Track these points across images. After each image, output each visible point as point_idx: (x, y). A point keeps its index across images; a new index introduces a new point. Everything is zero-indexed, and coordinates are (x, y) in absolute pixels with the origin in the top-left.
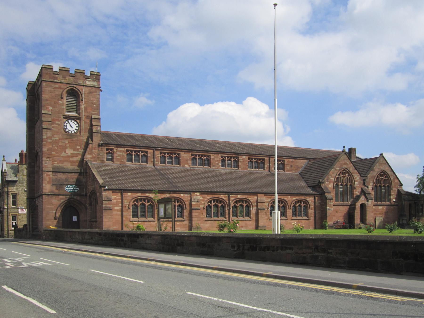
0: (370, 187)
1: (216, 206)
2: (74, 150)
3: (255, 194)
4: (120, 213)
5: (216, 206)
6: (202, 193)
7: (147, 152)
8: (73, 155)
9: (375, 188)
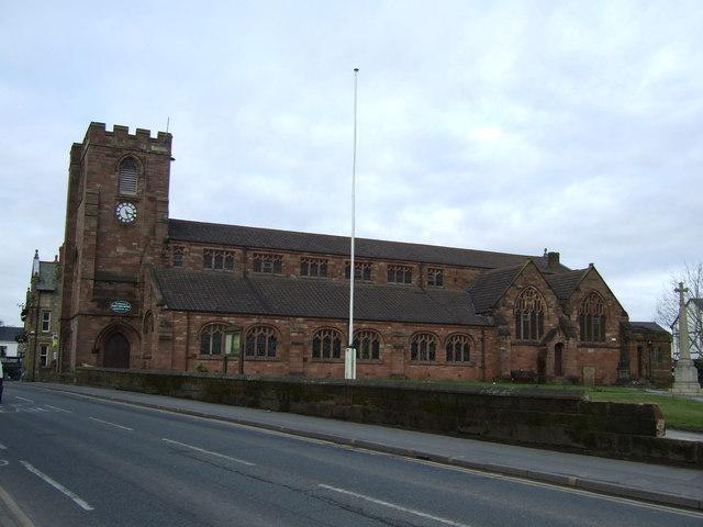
0: (574, 317)
1: (327, 340)
2: (128, 248)
3: (390, 321)
4: (184, 347)
5: (327, 340)
6: (308, 318)
7: (233, 253)
8: (125, 256)
9: (581, 319)
